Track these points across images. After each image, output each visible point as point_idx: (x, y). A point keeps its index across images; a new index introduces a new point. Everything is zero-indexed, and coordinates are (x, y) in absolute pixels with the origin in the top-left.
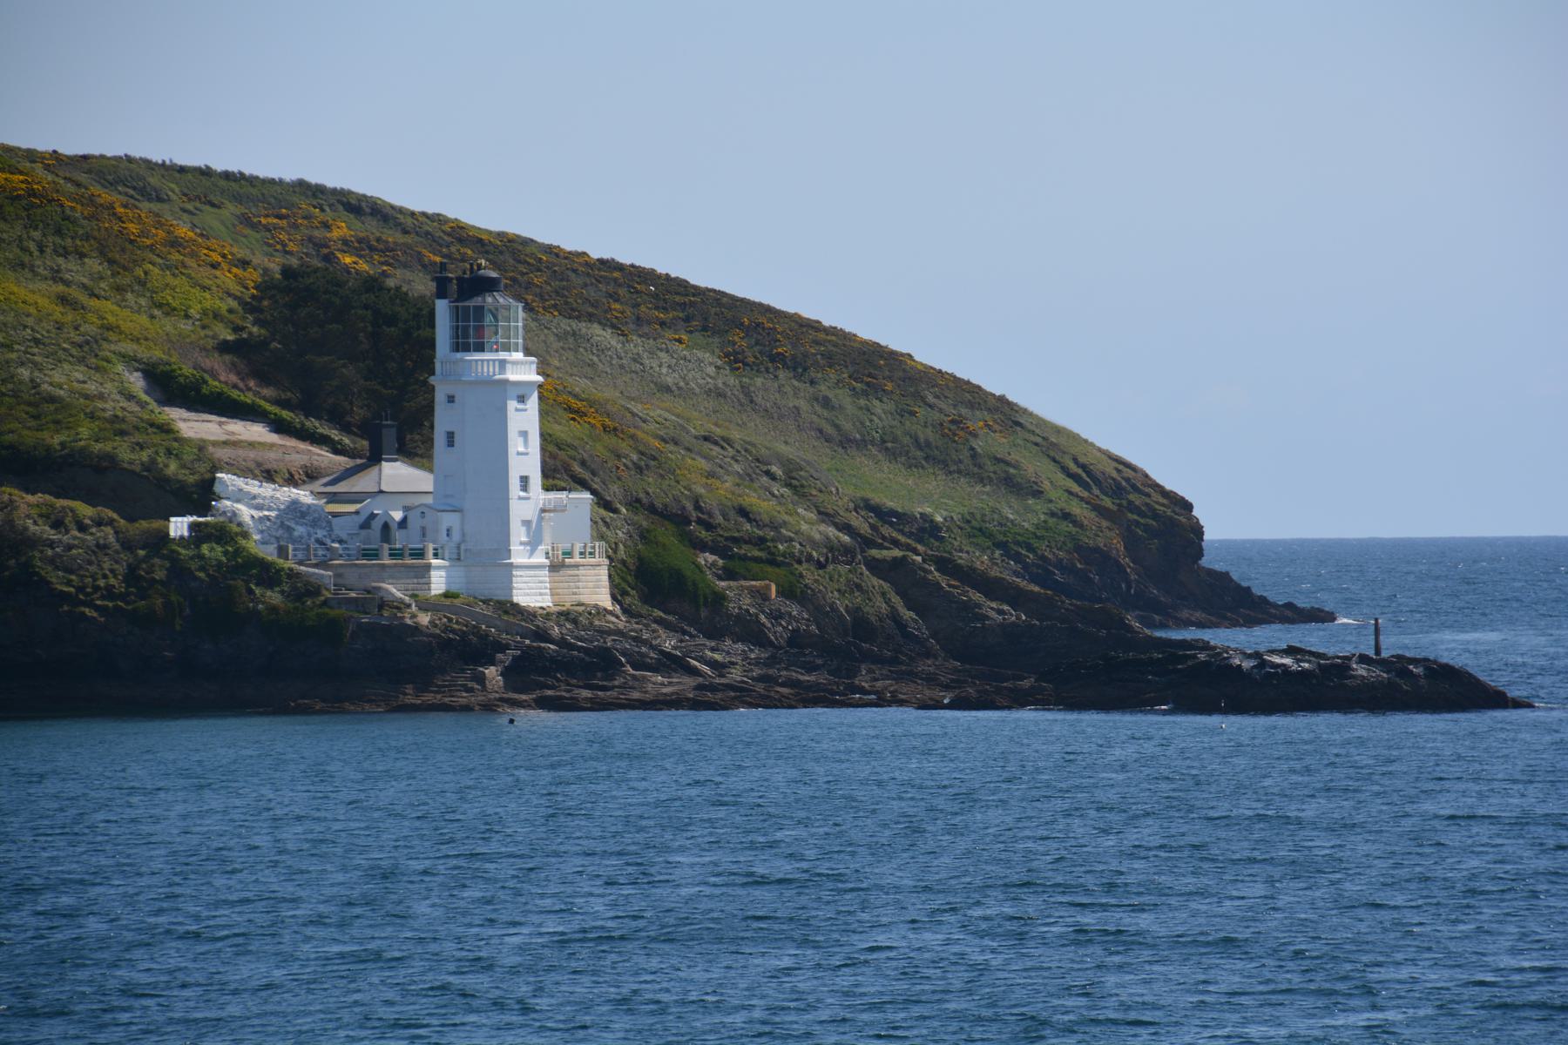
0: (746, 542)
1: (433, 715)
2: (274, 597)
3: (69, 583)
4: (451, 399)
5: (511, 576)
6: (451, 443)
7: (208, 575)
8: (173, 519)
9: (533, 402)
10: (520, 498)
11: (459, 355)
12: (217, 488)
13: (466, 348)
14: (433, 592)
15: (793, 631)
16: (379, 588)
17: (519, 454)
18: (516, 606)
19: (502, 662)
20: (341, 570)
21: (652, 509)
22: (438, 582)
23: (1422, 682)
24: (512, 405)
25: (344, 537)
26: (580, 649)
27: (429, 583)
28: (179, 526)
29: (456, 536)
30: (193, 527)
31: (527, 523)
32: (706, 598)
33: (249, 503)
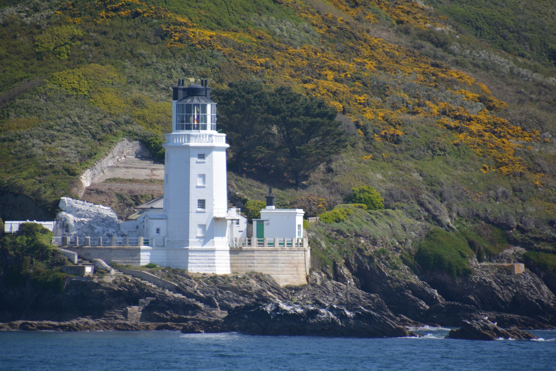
0: (543, 240)
1: (121, 332)
2: (41, 266)
5: (188, 256)
7: (15, 253)
10: (197, 212)
12: (61, 205)
14: (141, 264)
15: (517, 293)
16: (96, 261)
17: (197, 187)
19: (143, 304)
20: (89, 251)
21: (487, 220)
22: (145, 258)
23: (352, 321)
24: (194, 160)
25: (126, 232)
27: (139, 259)
29: (163, 232)
30: (21, 226)
31: (203, 226)
32: (458, 271)
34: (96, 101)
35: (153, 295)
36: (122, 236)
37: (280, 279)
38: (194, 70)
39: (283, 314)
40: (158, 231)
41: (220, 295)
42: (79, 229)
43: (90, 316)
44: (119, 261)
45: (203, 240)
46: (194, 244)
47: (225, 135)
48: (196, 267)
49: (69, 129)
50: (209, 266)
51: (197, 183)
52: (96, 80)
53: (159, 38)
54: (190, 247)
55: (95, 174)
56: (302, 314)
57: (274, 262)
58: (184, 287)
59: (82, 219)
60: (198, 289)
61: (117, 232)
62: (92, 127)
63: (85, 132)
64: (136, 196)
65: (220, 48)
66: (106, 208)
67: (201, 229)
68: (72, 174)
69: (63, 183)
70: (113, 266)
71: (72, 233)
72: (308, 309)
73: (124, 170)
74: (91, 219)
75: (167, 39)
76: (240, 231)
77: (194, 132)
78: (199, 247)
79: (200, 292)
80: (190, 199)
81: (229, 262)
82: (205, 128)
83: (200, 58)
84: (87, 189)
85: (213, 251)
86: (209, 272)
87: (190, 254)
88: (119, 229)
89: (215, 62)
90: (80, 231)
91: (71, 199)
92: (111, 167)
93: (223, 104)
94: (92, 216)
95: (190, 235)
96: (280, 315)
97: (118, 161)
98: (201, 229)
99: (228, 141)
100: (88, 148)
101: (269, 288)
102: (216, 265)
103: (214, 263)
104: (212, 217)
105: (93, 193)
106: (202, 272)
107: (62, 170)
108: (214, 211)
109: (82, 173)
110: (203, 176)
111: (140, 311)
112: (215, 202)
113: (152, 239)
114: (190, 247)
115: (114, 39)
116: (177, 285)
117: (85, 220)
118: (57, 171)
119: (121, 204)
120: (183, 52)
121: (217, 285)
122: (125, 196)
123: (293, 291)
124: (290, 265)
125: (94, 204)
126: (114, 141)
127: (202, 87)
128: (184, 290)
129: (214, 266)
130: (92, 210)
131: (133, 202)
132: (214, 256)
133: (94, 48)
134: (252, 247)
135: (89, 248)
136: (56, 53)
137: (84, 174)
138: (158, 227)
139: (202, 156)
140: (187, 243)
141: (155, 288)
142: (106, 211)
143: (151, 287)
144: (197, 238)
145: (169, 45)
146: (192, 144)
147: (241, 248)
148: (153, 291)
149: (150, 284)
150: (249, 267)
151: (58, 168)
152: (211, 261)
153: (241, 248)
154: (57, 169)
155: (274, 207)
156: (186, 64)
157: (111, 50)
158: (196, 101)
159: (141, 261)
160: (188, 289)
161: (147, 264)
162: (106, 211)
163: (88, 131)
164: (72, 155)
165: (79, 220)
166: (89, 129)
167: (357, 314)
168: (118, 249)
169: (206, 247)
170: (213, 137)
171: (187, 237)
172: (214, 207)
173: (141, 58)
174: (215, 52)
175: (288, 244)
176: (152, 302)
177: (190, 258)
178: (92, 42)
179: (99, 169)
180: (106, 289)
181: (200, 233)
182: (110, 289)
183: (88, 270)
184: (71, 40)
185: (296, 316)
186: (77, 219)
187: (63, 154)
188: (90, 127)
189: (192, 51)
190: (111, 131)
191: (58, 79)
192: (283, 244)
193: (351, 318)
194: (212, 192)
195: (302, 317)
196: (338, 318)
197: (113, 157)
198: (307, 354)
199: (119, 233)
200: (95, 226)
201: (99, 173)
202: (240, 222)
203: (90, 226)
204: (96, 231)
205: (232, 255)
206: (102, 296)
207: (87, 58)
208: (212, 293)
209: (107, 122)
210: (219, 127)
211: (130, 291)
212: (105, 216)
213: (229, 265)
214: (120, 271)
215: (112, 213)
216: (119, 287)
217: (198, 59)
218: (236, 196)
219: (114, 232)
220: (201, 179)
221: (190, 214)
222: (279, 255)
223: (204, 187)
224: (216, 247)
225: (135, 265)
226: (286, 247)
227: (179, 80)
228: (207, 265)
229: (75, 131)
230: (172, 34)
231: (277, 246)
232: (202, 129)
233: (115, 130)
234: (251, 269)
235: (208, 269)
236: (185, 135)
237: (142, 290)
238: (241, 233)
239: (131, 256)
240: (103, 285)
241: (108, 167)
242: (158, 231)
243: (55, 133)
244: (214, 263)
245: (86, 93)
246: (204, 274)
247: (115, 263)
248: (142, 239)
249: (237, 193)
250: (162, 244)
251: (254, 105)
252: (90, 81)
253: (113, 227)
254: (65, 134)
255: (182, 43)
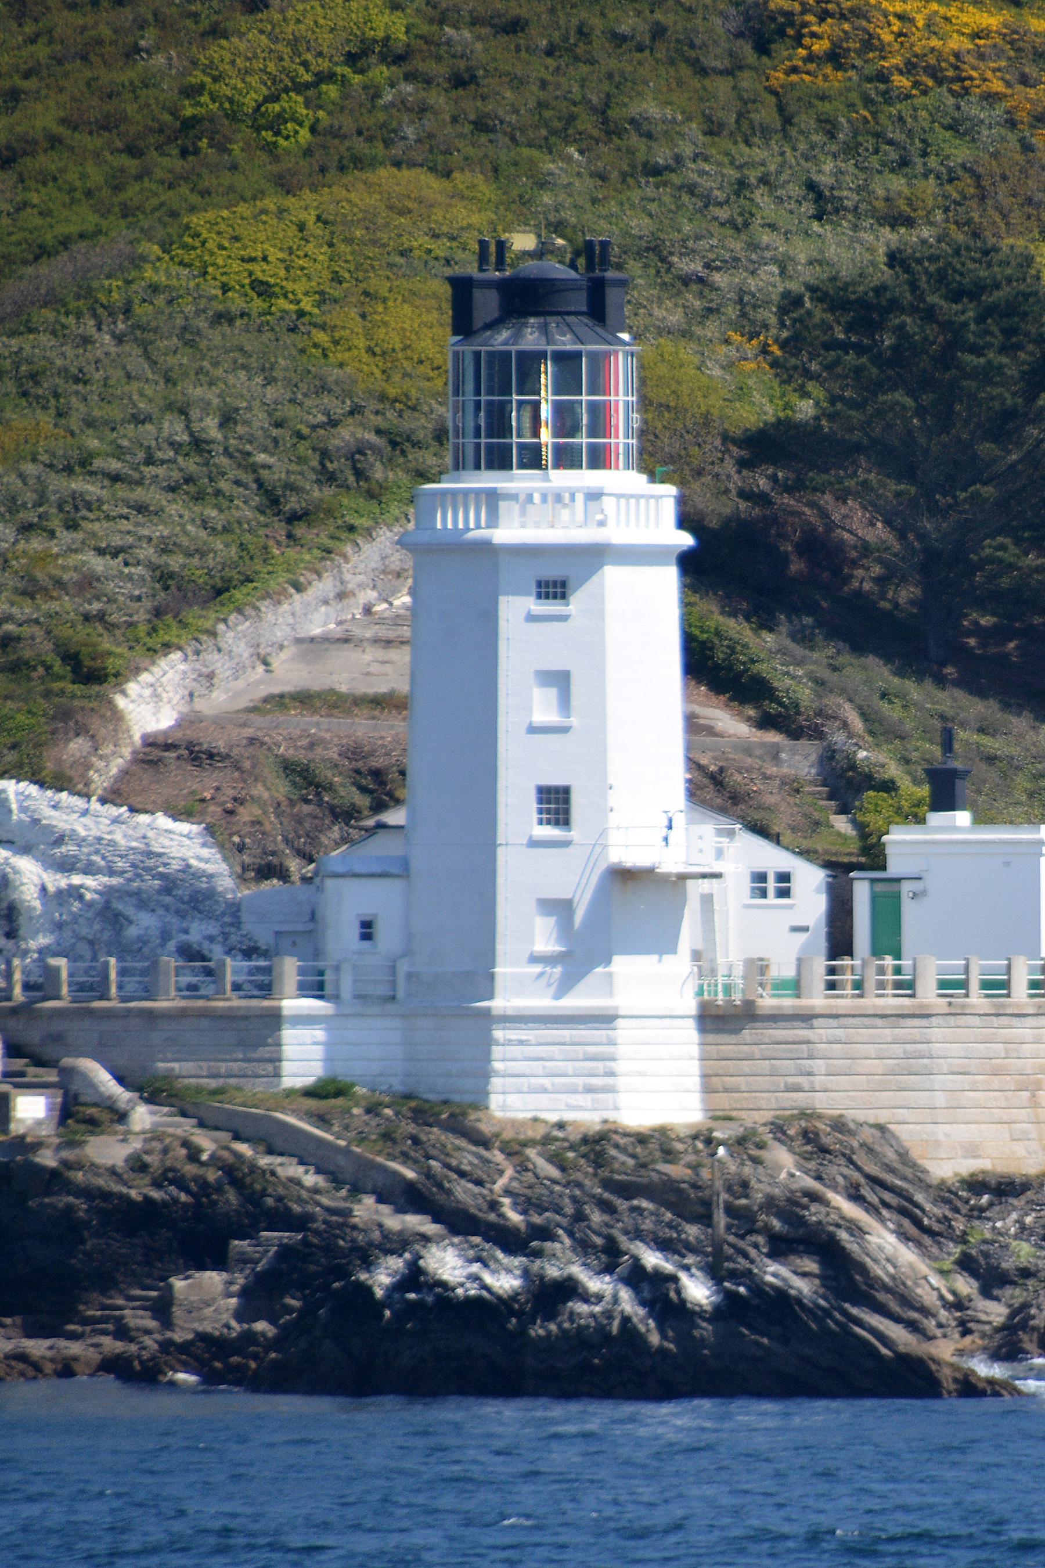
5: (489, 1042)
10: (534, 843)
14: (288, 1082)
17: (534, 730)
19: (244, 1260)
20: (58, 1026)
22: (303, 1055)
23: (705, 1330)
27: (276, 1060)
29: (388, 938)
31: (559, 908)
34: (336, 343)
35: (301, 1223)
36: (249, 953)
37: (937, 1144)
38: (859, 190)
39: (430, 1299)
40: (367, 930)
41: (597, 1217)
42: (59, 926)
43: (18, 1320)
44: (183, 1070)
45: (558, 970)
46: (518, 985)
47: (670, 490)
48: (527, 1091)
49: (160, 471)
50: (589, 1090)
51: (530, 710)
52: (374, 242)
53: (746, 50)
54: (499, 1004)
55: (211, 676)
56: (514, 1297)
57: (914, 1067)
58: (440, 1186)
59: (76, 880)
60: (507, 1192)
61: (226, 936)
62: (270, 460)
63: (237, 483)
64: (377, 774)
65: (997, 86)
66: (184, 827)
67: (552, 920)
68: (93, 674)
69: (21, 718)
70: (153, 1092)
71: (33, 944)
72: (542, 1277)
73: (370, 655)
74: (115, 881)
75: (781, 50)
76: (796, 929)
77: (520, 481)
78: (542, 1002)
79: (515, 1206)
80: (501, 784)
81: (694, 1067)
82: (599, 459)
83: (898, 136)
84: (151, 742)
85: (606, 1019)
86: (586, 1114)
87: (498, 1034)
88: (237, 924)
89: (960, 153)
90: (67, 933)
91: (33, 790)
92: (312, 640)
93: (844, 346)
94: (120, 864)
95: (500, 947)
96: (420, 1304)
97: (368, 610)
98: (552, 920)
100: (223, 550)
101: (857, 1187)
102: (621, 1082)
103: (612, 1074)
104: (602, 866)
105: (175, 764)
106: (553, 1117)
107: (51, 658)
108: (614, 838)
109: (137, 671)
110: (560, 680)
111: (230, 1295)
112: (613, 799)
113: (337, 969)
114: (499, 1004)
115: (549, 52)
116: (410, 1174)
117: (90, 882)
118: (26, 663)
119: (307, 809)
120: (826, 107)
121: (604, 1173)
122: (326, 774)
123: (985, 1199)
124: (996, 1082)
125: (133, 810)
126: (357, 522)
127: (572, 274)
128: (441, 1198)
129: (611, 1090)
130: (118, 837)
131: (362, 801)
132: (612, 1042)
133: (437, 98)
134: (804, 1002)
135: (59, 1013)
136: (266, 122)
137: (145, 677)
138: (366, 910)
139: (555, 590)
140: (487, 985)
141: (316, 1190)
142: (182, 843)
143: (298, 1183)
144: (534, 959)
145: (778, 77)
146: (505, 534)
147: (749, 1004)
148: (300, 1200)
149: (296, 1170)
150: (788, 1089)
151: (39, 646)
152: (600, 1066)
153: (749, 1004)
154: (27, 654)
155: (963, 818)
156: (828, 166)
157: (506, 103)
158: (531, 339)
159: (287, 1067)
160: (463, 1192)
161: (309, 1081)
162: (182, 843)
163: (247, 478)
164: (126, 587)
165: (63, 883)
166: (254, 468)
167: (731, 1297)
168: (182, 1014)
169: (575, 1001)
170: (608, 503)
171: (487, 956)
172: (613, 819)
173: (634, 140)
174: (973, 110)
175: (986, 985)
176: (286, 1252)
177: (497, 1051)
178: (438, 70)
179: (242, 650)
180: (87, 1193)
181: (544, 937)
182: (107, 1196)
183: (31, 1109)
184: (351, 59)
185: (485, 1310)
186: (56, 881)
187: (88, 583)
188: (262, 457)
189: (868, 101)
190: (359, 474)
191: (203, 243)
192: (964, 985)
193: (701, 1314)
194: (604, 751)
195: (512, 1313)
196: (650, 1314)
197: (341, 596)
198: (152, 1473)
199: (234, 939)
200: (130, 911)
201: (238, 671)
202: (795, 885)
203: (109, 912)
204: (132, 932)
205: (711, 1038)
206: (68, 1227)
207: (389, 136)
208: (558, 1210)
209: (346, 435)
210: (652, 461)
211: (198, 1204)
212: (175, 865)
213: (695, 1082)
214: (184, 1114)
215: (205, 852)
216: (157, 1184)
217: (890, 142)
218: (853, 766)
219: (211, 939)
220: (553, 693)
221: (501, 852)
222: (935, 1033)
223: (564, 730)
224: (622, 1001)
225: (259, 1087)
226: (977, 998)
227: (483, 245)
228: (580, 1081)
229: (189, 480)
230: (805, 24)
231: (928, 994)
232: (522, 466)
233: (378, 473)
234: (800, 1099)
235: (582, 1100)
236: (477, 492)
237: (253, 1198)
238: (802, 937)
239: (241, 1043)
240: (79, 1176)
241: (299, 641)
242: (367, 930)
243: (92, 489)
244: (612, 1074)
245: (307, 304)
246: (561, 1125)
247: (169, 1076)
248: (290, 968)
249: (862, 754)
250: (382, 990)
251: (976, 350)
252: (342, 247)
253: (208, 916)
254: (139, 494)
255: (839, 67)
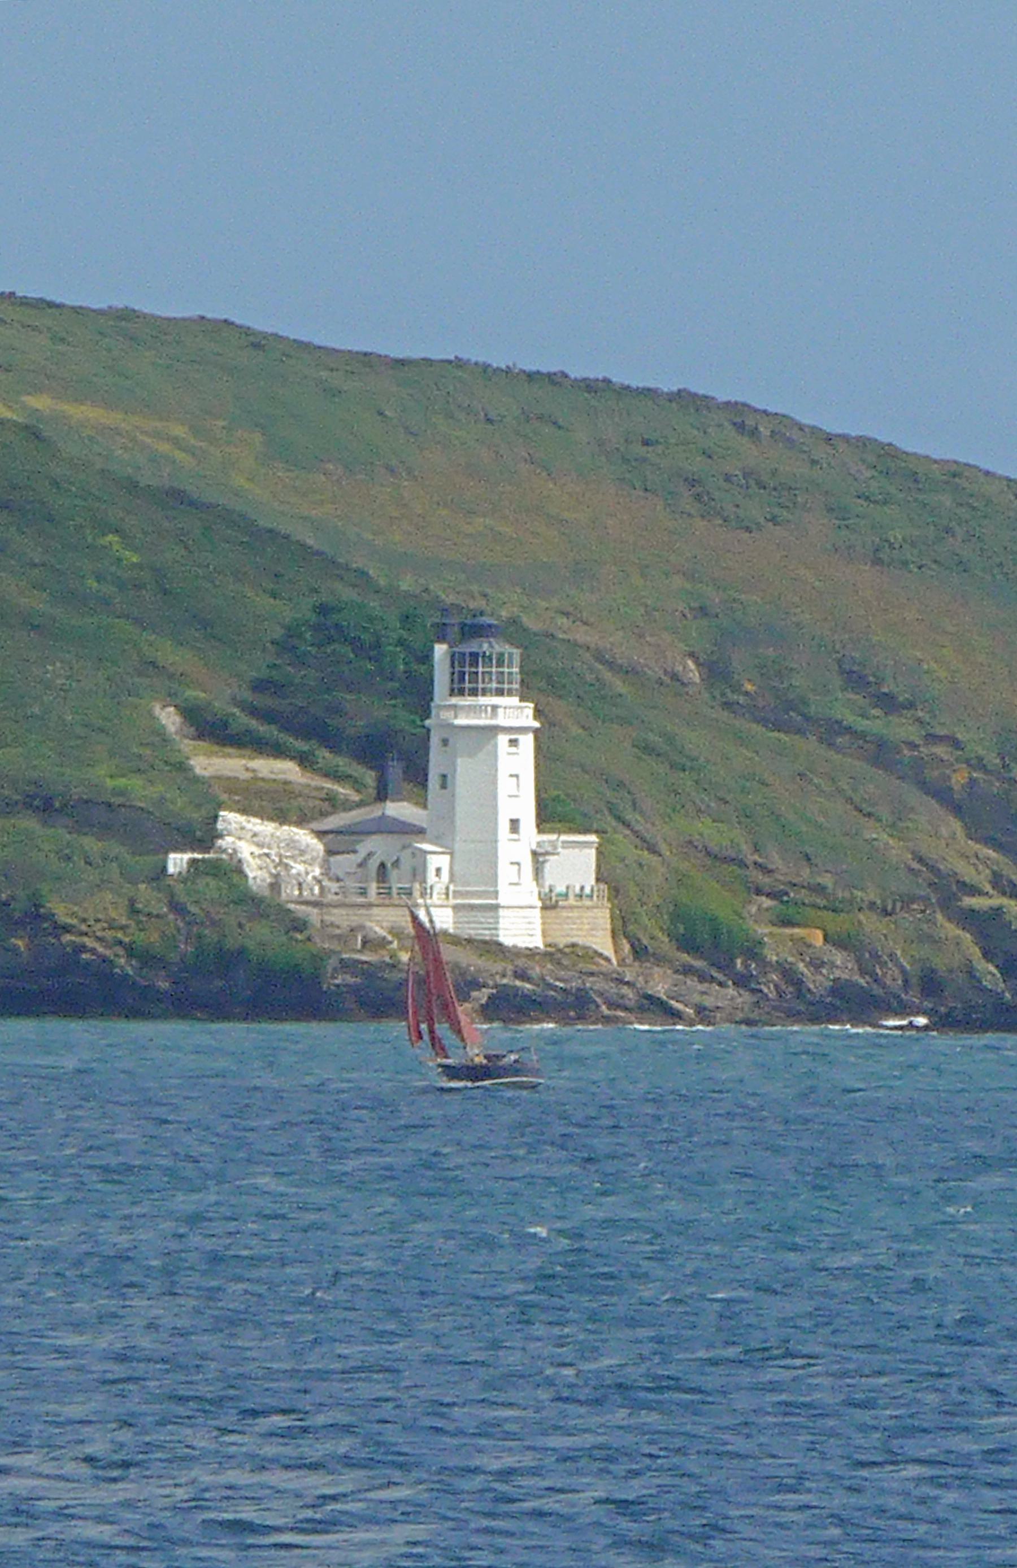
3: (73, 914)
4: (445, 742)
6: (444, 786)
8: (172, 856)
9: (527, 742)
11: (454, 700)
12: (220, 825)
13: (461, 692)
15: (834, 980)
18: (500, 945)
19: (477, 999)
25: (341, 875)
26: (555, 988)
28: (177, 862)
33: (249, 841)
85: (496, 907)
99: (538, 713)
